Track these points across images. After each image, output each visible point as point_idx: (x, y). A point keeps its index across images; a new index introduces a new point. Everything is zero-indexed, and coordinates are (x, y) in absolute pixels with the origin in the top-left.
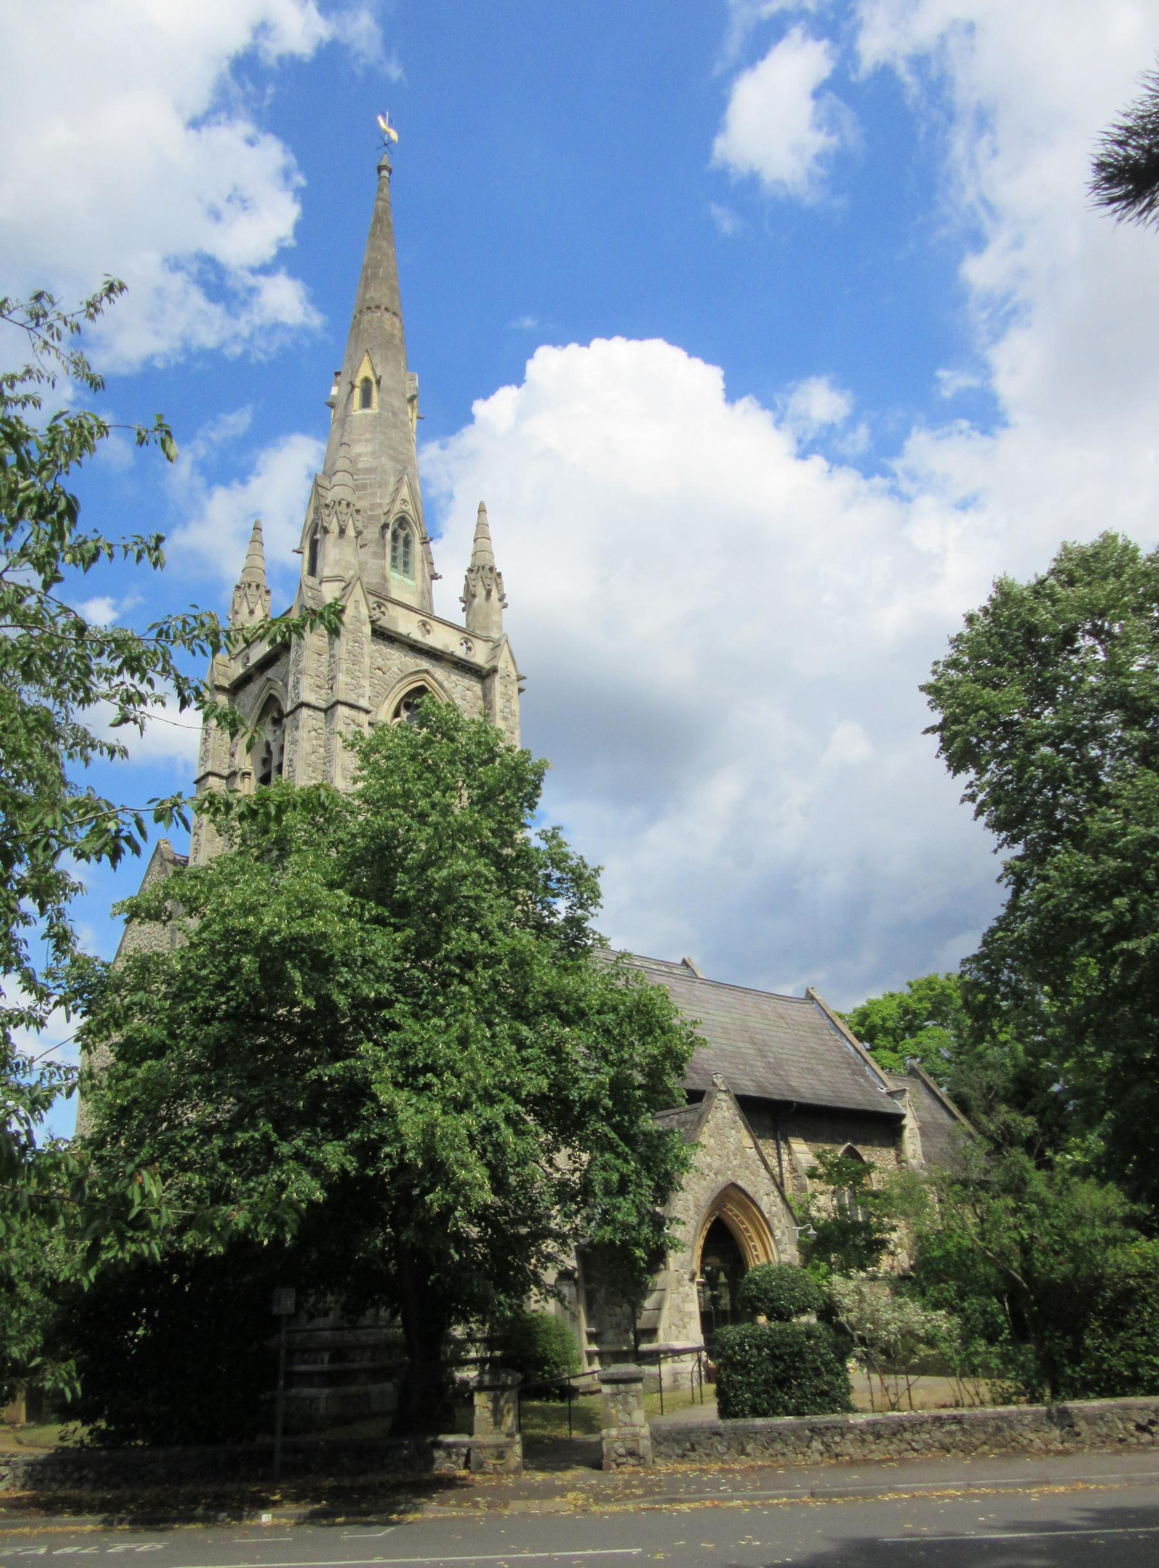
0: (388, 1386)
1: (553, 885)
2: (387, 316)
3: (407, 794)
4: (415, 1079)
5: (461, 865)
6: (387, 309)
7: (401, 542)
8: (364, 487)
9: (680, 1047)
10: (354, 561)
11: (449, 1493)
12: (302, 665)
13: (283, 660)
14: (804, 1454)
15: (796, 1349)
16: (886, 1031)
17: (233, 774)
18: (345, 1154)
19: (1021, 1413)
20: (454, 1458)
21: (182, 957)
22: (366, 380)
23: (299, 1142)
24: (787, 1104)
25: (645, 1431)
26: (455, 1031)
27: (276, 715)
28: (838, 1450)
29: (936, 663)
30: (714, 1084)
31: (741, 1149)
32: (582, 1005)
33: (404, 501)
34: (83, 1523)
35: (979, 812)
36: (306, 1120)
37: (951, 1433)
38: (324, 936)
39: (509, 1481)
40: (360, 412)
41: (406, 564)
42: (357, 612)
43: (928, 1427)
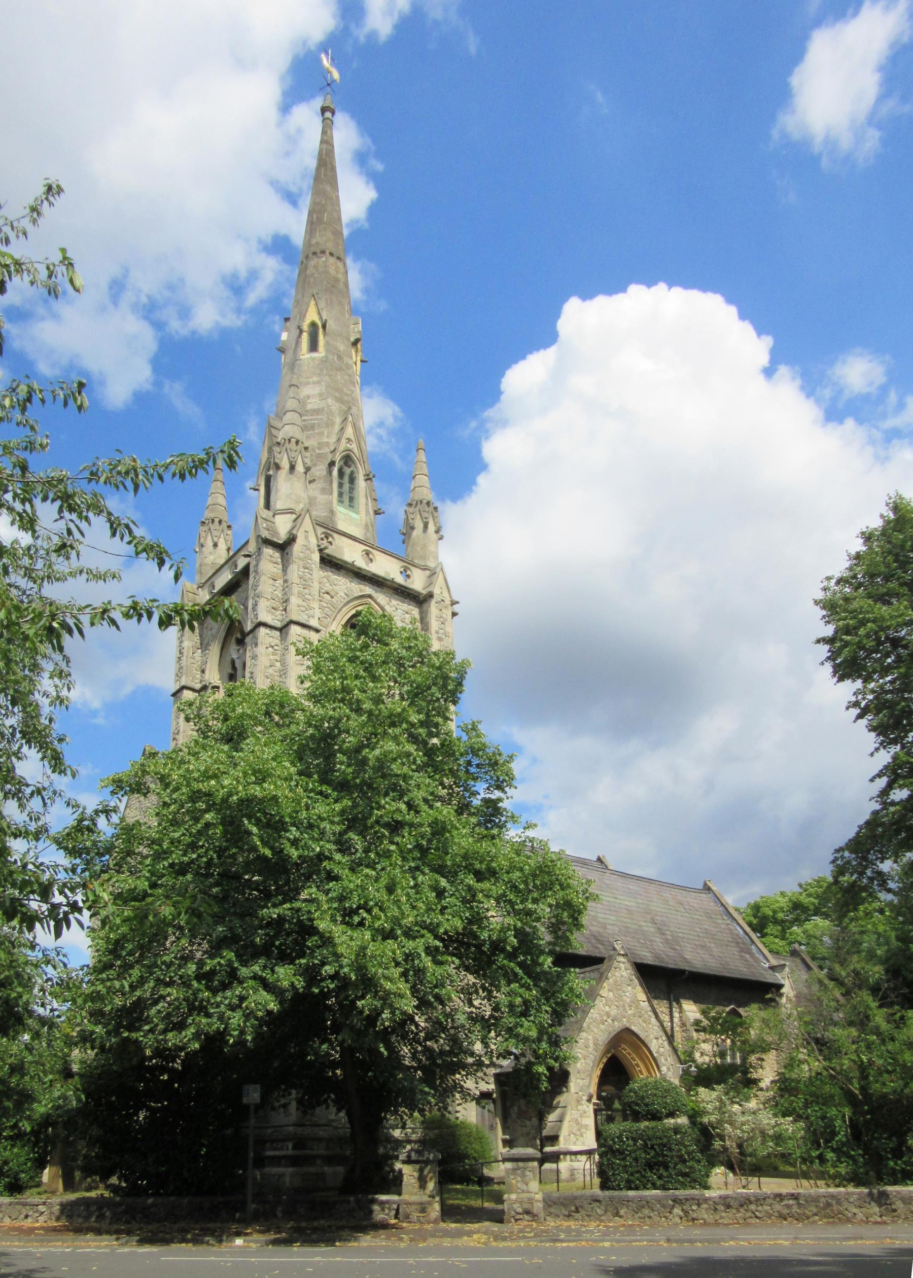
0: (341, 1169)
1: (472, 770)
2: (332, 260)
3: (346, 690)
4: (351, 917)
5: (390, 746)
6: (331, 254)
7: (346, 479)
8: (312, 427)
9: (578, 900)
10: (304, 495)
11: (381, 1232)
12: (260, 589)
13: (244, 586)
14: (666, 1218)
15: (665, 1140)
16: (776, 922)
17: (204, 688)
18: (295, 975)
19: (848, 1194)
20: (387, 1211)
21: (157, 814)
22: (313, 325)
23: (256, 968)
24: (683, 972)
25: (539, 1197)
26: (384, 881)
27: (239, 636)
28: (695, 1215)
29: (828, 579)
30: (614, 949)
31: (635, 1002)
32: (494, 865)
33: (349, 440)
34: (102, 1241)
35: (860, 716)
36: (265, 951)
37: (788, 1206)
38: (275, 798)
39: (429, 1227)
40: (308, 356)
41: (351, 499)
42: (308, 542)
43: (769, 1201)
